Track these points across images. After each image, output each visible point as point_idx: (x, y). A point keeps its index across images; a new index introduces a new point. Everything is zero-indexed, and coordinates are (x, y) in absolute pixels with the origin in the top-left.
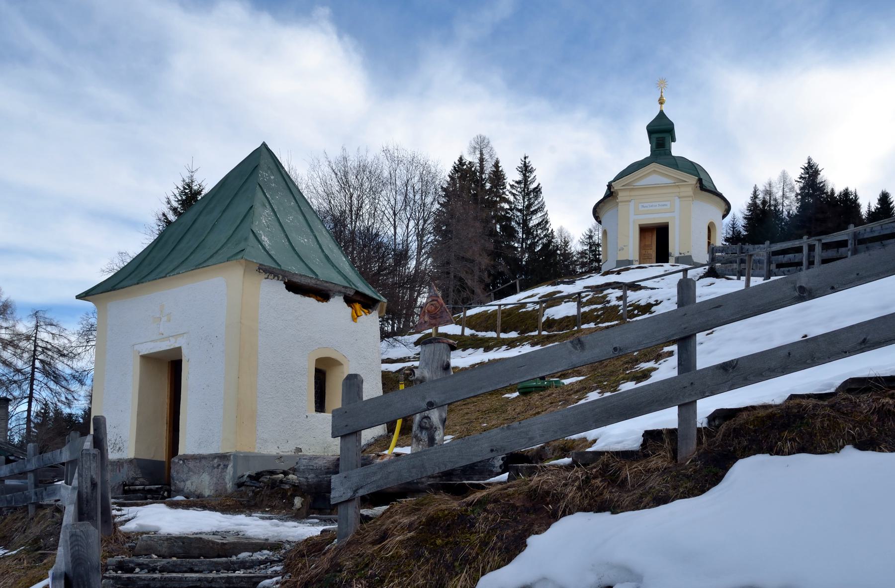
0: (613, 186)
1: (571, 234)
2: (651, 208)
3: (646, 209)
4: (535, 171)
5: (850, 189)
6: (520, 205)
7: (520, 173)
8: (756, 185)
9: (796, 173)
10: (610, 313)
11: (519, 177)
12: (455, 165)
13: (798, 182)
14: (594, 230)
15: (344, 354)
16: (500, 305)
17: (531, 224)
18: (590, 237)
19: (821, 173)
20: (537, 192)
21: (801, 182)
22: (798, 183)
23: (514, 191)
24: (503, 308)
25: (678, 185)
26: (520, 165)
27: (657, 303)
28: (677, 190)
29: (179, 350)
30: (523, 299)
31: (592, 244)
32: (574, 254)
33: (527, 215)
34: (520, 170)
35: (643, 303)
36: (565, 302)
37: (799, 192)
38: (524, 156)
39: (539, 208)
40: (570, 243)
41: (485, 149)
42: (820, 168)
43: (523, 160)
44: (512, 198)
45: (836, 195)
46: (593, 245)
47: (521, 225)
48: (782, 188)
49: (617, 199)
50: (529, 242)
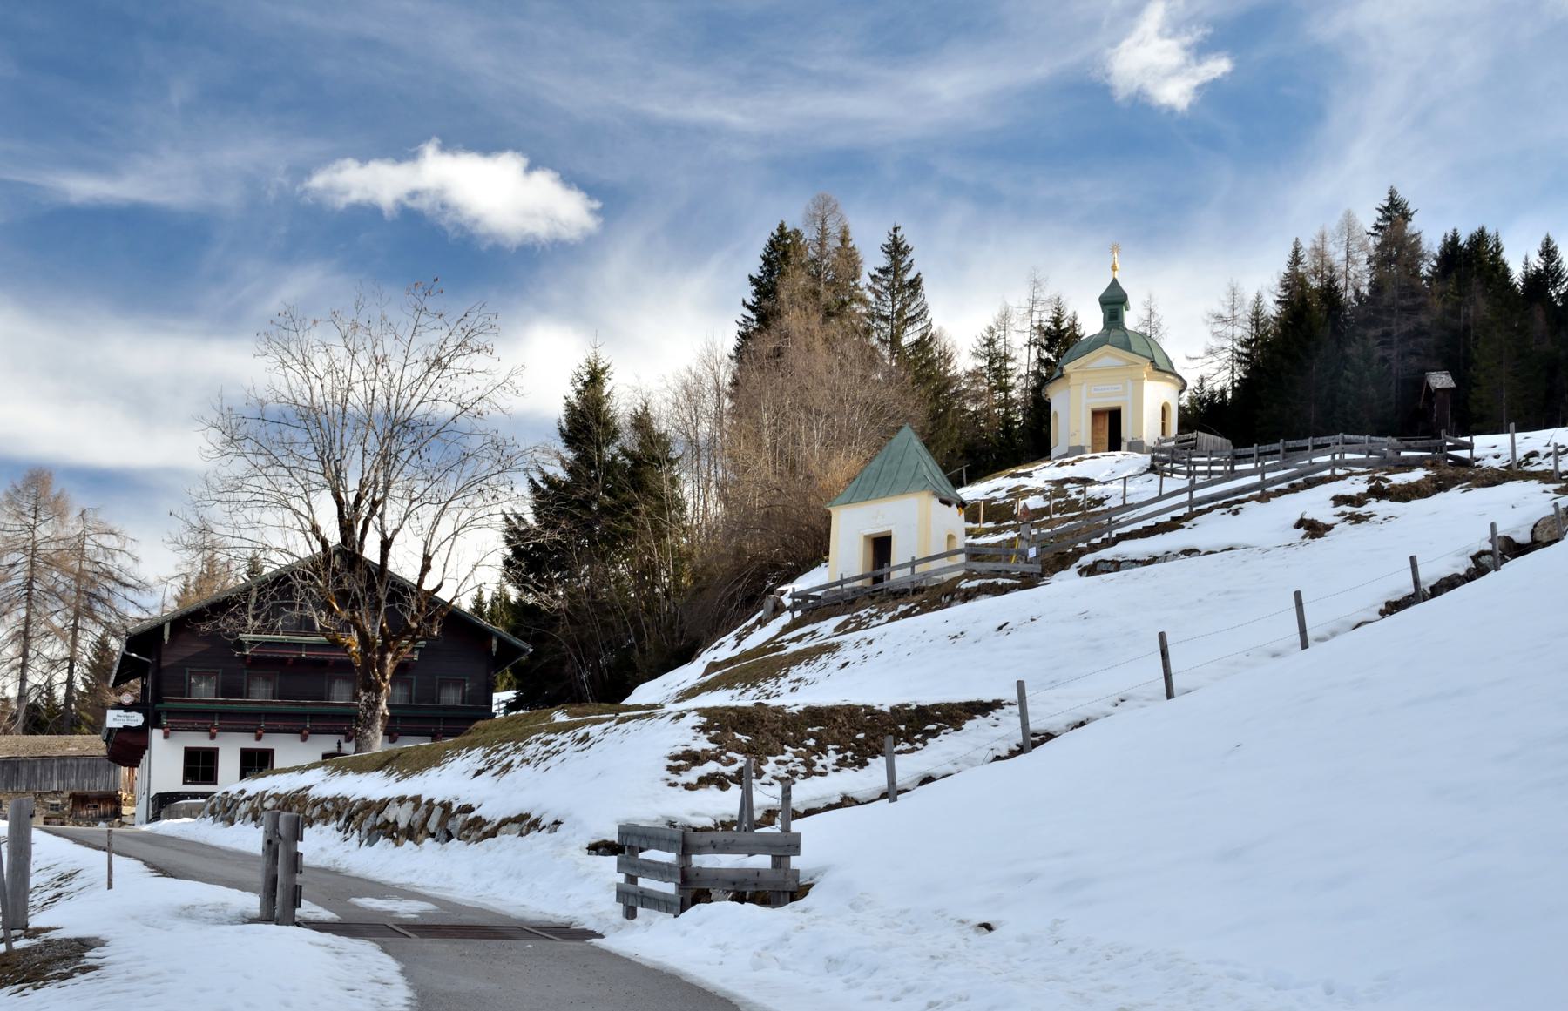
5: (1488, 231)
6: (886, 309)
7: (886, 255)
8: (1297, 239)
9: (1368, 218)
10: (1072, 505)
11: (884, 262)
12: (772, 238)
13: (1372, 234)
18: (991, 342)
19: (1413, 217)
21: (1376, 235)
22: (1372, 237)
23: (877, 287)
26: (887, 242)
27: (1108, 498)
29: (891, 531)
30: (992, 492)
35: (1097, 497)
37: (1373, 253)
38: (893, 226)
39: (918, 315)
41: (831, 216)
43: (892, 232)
44: (871, 297)
45: (1461, 242)
48: (1345, 244)
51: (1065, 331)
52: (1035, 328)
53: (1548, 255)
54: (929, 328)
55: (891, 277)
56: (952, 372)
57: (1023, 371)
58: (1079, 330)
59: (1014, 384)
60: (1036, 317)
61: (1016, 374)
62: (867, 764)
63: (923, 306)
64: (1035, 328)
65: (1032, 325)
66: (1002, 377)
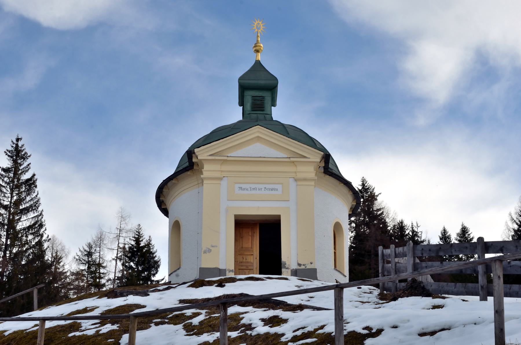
0: (197, 154)
1: (67, 247)
2: (253, 192)
3: (245, 192)
4: (30, 158)
6: (5, 199)
7: (9, 158)
14: (94, 245)
15: (198, 241)
16: (43, 320)
17: (20, 226)
18: (89, 254)
19: (378, 198)
20: (30, 186)
24: (49, 324)
25: (293, 162)
26: (10, 149)
28: (290, 169)
31: (92, 263)
32: (68, 274)
33: (14, 214)
34: (10, 154)
36: (157, 324)
38: (16, 137)
39: (31, 206)
40: (64, 259)
42: (376, 192)
43: (15, 142)
46: (93, 264)
47: (6, 227)
49: (202, 174)
50: (15, 250)
51: (143, 247)
52: (120, 248)
53: (445, 240)
54: (40, 217)
55: (11, 175)
56: (61, 270)
57: (112, 276)
58: (153, 248)
59: (104, 284)
60: (122, 240)
61: (107, 278)
62: (149, 295)
63: (36, 200)
64: (120, 248)
65: (118, 246)
66: (96, 278)
